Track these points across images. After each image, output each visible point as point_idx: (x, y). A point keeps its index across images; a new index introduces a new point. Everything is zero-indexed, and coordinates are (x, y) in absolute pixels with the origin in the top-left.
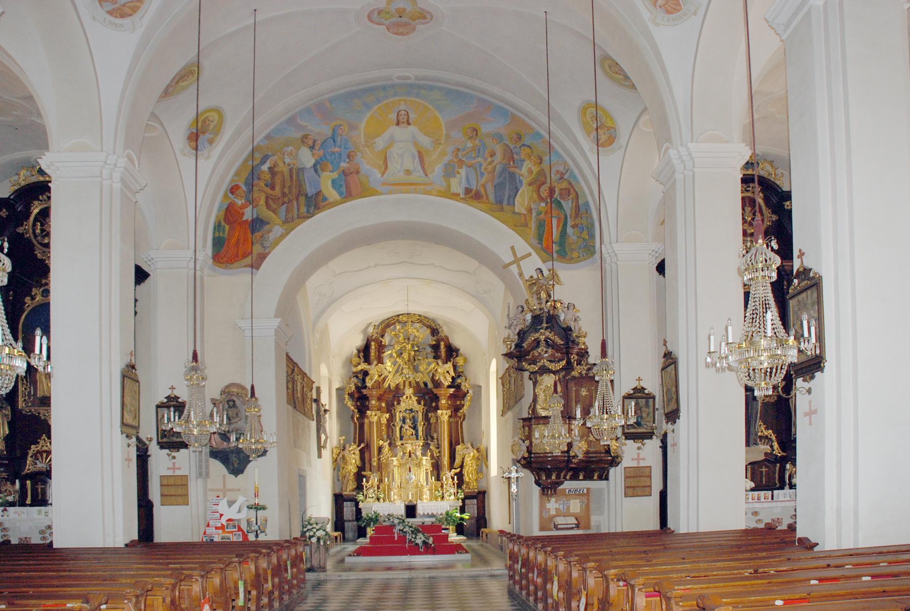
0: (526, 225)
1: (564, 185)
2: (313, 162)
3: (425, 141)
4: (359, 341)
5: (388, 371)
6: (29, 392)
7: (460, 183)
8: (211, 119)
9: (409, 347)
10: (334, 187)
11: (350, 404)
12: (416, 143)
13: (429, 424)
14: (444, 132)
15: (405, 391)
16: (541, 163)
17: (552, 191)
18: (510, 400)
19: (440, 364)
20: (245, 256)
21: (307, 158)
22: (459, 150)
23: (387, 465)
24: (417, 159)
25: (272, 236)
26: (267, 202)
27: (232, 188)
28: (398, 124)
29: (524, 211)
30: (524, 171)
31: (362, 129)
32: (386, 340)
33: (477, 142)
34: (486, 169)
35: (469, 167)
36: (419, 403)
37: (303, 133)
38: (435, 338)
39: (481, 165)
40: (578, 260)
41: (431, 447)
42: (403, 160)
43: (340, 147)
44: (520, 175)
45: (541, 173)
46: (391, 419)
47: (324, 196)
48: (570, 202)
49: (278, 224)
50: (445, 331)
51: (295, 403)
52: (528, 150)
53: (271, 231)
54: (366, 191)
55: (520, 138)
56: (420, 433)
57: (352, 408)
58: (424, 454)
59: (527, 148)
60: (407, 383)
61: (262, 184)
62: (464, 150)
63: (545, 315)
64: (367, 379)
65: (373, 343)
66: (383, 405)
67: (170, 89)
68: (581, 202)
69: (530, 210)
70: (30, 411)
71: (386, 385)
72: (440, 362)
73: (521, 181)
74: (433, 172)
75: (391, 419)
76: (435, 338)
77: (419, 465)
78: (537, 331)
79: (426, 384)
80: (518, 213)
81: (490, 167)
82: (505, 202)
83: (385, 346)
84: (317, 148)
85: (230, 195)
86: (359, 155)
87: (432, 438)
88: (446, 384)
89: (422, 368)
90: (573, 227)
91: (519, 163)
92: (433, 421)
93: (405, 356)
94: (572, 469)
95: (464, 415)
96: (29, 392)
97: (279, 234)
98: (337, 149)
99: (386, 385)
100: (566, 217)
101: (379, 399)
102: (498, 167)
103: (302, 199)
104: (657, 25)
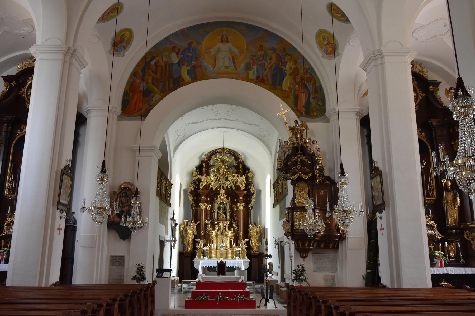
0: (288, 97)
1: (308, 76)
2: (178, 60)
3: (236, 51)
4: (196, 162)
5: (211, 180)
6: (12, 186)
7: (254, 73)
8: (126, 35)
9: (223, 167)
10: (188, 74)
11: (190, 198)
12: (230, 51)
13: (233, 211)
15: (221, 193)
16: (295, 64)
17: (302, 79)
18: (279, 197)
21: (175, 59)
22: (253, 56)
24: (231, 61)
26: (152, 81)
27: (135, 73)
28: (222, 42)
29: (287, 90)
30: (287, 68)
31: (204, 44)
32: (211, 162)
34: (267, 66)
35: (259, 65)
36: (228, 199)
38: (237, 162)
39: (264, 64)
40: (317, 117)
41: (234, 225)
42: (224, 61)
45: (296, 69)
46: (212, 208)
47: (183, 79)
48: (312, 85)
51: (161, 195)
52: (289, 57)
53: (154, 97)
55: (285, 51)
56: (228, 217)
57: (191, 200)
58: (230, 229)
59: (288, 56)
60: (222, 187)
61: (150, 72)
62: (256, 56)
63: (300, 147)
64: (201, 184)
65: (204, 164)
66: (209, 199)
67: (105, 17)
68: (317, 85)
69: (290, 89)
70: (11, 197)
71: (210, 188)
73: (286, 73)
75: (212, 208)
76: (237, 162)
77: (227, 236)
78: (296, 156)
79: (231, 187)
80: (284, 91)
81: (269, 65)
83: (210, 166)
84: (180, 53)
85: (134, 77)
87: (234, 220)
88: (242, 188)
89: (229, 179)
90: (313, 98)
91: (285, 64)
92: (235, 209)
94: (317, 240)
95: (252, 207)
96: (12, 186)
97: (158, 99)
98: (190, 54)
99: (210, 188)
100: (309, 93)
101: (207, 196)
104: (324, 58)
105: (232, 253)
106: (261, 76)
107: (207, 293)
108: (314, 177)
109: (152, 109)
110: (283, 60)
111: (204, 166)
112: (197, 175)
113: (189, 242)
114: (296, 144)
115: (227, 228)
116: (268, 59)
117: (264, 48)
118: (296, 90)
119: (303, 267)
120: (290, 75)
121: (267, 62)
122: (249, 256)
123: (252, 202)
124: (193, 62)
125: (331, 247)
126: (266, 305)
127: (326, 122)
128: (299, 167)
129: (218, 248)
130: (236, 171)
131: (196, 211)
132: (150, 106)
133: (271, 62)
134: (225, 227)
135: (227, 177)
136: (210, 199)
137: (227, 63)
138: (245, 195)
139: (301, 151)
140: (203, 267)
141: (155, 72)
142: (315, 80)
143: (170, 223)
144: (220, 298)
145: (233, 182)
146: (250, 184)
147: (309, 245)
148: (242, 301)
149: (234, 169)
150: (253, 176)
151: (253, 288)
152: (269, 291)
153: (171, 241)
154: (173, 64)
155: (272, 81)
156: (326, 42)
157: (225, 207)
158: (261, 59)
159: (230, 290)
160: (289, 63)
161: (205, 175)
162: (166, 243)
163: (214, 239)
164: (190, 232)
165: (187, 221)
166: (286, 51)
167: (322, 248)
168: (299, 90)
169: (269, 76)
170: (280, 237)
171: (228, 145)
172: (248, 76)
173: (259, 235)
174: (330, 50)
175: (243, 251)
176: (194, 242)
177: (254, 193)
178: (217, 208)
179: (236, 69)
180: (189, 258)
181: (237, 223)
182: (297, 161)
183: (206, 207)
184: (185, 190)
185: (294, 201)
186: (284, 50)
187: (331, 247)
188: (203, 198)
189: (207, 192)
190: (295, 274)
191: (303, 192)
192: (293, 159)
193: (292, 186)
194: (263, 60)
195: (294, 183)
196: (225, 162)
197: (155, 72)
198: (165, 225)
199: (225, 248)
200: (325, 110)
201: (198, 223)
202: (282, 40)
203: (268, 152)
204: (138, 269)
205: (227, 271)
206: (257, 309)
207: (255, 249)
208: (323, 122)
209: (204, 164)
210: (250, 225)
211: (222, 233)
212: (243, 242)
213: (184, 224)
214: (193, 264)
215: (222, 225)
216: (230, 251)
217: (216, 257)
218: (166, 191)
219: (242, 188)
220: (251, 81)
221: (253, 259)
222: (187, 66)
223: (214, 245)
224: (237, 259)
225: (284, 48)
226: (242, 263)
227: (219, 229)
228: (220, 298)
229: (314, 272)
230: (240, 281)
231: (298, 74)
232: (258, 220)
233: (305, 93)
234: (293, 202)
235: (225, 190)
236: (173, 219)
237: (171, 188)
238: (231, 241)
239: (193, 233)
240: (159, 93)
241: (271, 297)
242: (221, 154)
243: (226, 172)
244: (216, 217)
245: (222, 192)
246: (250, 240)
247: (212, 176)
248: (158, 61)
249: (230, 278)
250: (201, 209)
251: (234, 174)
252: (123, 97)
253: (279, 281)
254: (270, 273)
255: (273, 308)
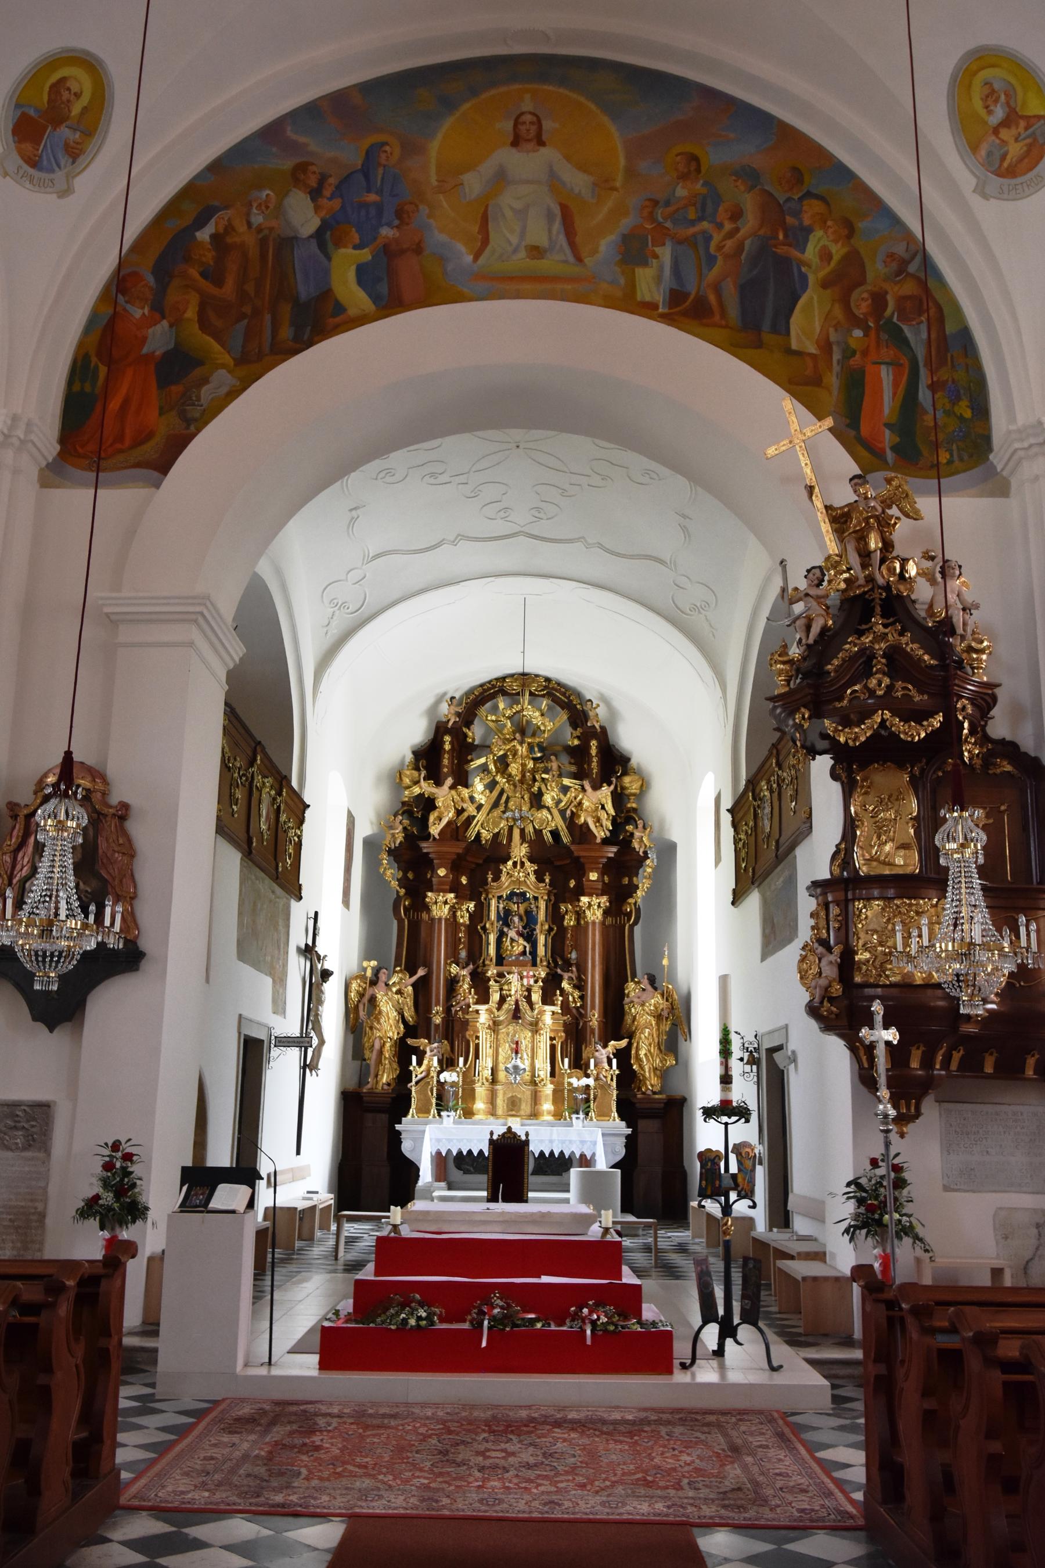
0: (817, 381)
1: (909, 288)
2: (315, 223)
3: (577, 181)
5: (472, 801)
7: (659, 279)
8: (75, 87)
9: (522, 750)
10: (360, 282)
11: (391, 874)
12: (554, 183)
13: (562, 930)
14: (622, 162)
17: (879, 300)
18: (760, 852)
19: (588, 787)
20: (138, 443)
21: (303, 216)
22: (655, 203)
23: (465, 1024)
24: (557, 225)
25: (206, 393)
28: (516, 143)
29: (812, 349)
30: (811, 253)
32: (476, 733)
33: (699, 186)
34: (719, 248)
36: (540, 879)
37: (299, 160)
39: (708, 239)
41: (565, 985)
42: (524, 224)
43: (380, 192)
44: (801, 263)
45: (853, 263)
46: (478, 916)
48: (924, 328)
49: (223, 366)
50: (600, 715)
53: (205, 381)
54: (433, 293)
56: (541, 951)
57: (394, 884)
58: (547, 1000)
59: (815, 202)
60: (516, 833)
61: (194, 272)
62: (668, 203)
64: (432, 817)
65: (447, 738)
66: (464, 880)
68: (950, 328)
69: (826, 347)
71: (471, 834)
72: (587, 785)
73: (804, 278)
74: (595, 251)
75: (478, 916)
77: (535, 1027)
79: (555, 834)
80: (798, 353)
81: (729, 243)
82: (766, 325)
84: (327, 193)
86: (424, 209)
88: (600, 834)
89: (548, 799)
91: (800, 236)
92: (570, 921)
93: (514, 769)
94: (969, 1038)
97: (224, 390)
98: (372, 197)
99: (471, 834)
101: (456, 868)
102: (747, 243)
103: (286, 310)
104: (985, 196)
105: (558, 1095)
106: (692, 287)
107: (430, 1294)
108: (947, 739)
109: (193, 436)
110: (790, 220)
111: (447, 747)
112: (416, 783)
113: (381, 1052)
114: (862, 581)
115: (536, 997)
116: (722, 214)
117: (703, 169)
118: (854, 353)
119: (897, 1169)
120: (825, 284)
121: (720, 226)
122: (627, 1110)
123: (639, 893)
124: (386, 232)
125: (1030, 1072)
126: (719, 1353)
127: (992, 494)
128: (879, 682)
129: (502, 1075)
130: (573, 769)
131: (415, 927)
132: (188, 422)
133: (737, 230)
134: (529, 990)
135: (540, 794)
136: (469, 879)
137: (538, 233)
138: (610, 865)
139: (883, 617)
140: (439, 1153)
141: (214, 275)
142: (940, 309)
143: (296, 968)
144: (493, 1319)
145: (562, 812)
146: (630, 820)
147: (927, 1063)
148: (601, 1334)
149: (565, 759)
150: (645, 785)
151: (647, 1249)
152: (737, 1277)
153: (301, 1042)
154: (295, 238)
155: (745, 313)
156: (999, 113)
157: (528, 913)
158: (692, 215)
159: (545, 1279)
160: (819, 233)
161: (449, 781)
162: (275, 1052)
163: (485, 1039)
164: (387, 1007)
165: (374, 963)
166: (805, 179)
167: (988, 1077)
168: (865, 353)
169: (730, 290)
170: (761, 1031)
171: (544, 663)
172: (632, 286)
173: (666, 1026)
174: (1015, 150)
175: (603, 1087)
176: (404, 1052)
177: (646, 856)
178: (499, 917)
179: (579, 260)
180: (384, 1117)
181: (579, 978)
182: (873, 656)
183: (453, 910)
184: (370, 844)
185: (849, 852)
186: (797, 176)
187: (1030, 1072)
188: (442, 872)
189: (458, 848)
190: (860, 1202)
191: (891, 814)
192: (851, 647)
193: (836, 788)
194: (701, 219)
195: (850, 767)
196: (529, 732)
197: (214, 275)
198: (271, 973)
199: (527, 1076)
200: (987, 439)
201: (421, 972)
202: (786, 135)
203: (708, 673)
204: (108, 1166)
205: (536, 1172)
206: (680, 1377)
207: (652, 1082)
208: (981, 495)
209: (447, 738)
210: (631, 985)
211: (516, 1014)
212: (603, 1053)
213: (363, 977)
214: (396, 1139)
215: (515, 986)
216: (548, 1089)
217: (493, 1113)
218: (277, 828)
219: (600, 834)
220: (647, 309)
221: (642, 1124)
222: (355, 248)
223: (485, 1064)
224: (578, 1122)
225: (796, 170)
226: (595, 1139)
227: (503, 1000)
228: (493, 1319)
229: (946, 1188)
230: (594, 1232)
231: (862, 282)
232: (665, 962)
233: (894, 364)
234: (843, 855)
235: (531, 844)
236: (309, 951)
237: (301, 821)
238: (553, 1048)
239: (401, 1013)
240: (232, 363)
241: (750, 1317)
242: (514, 697)
243: (534, 771)
244: (492, 951)
245: (520, 851)
246: (630, 1044)
247: (478, 785)
248: (229, 228)
249: (543, 1218)
250: (433, 919)
251: (566, 782)
252: (70, 382)
253: (761, 1226)
254: (740, 1197)
255: (760, 1377)
